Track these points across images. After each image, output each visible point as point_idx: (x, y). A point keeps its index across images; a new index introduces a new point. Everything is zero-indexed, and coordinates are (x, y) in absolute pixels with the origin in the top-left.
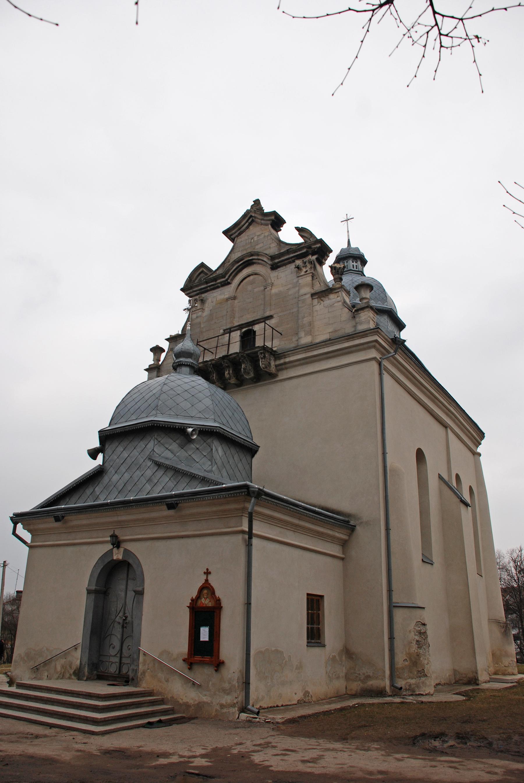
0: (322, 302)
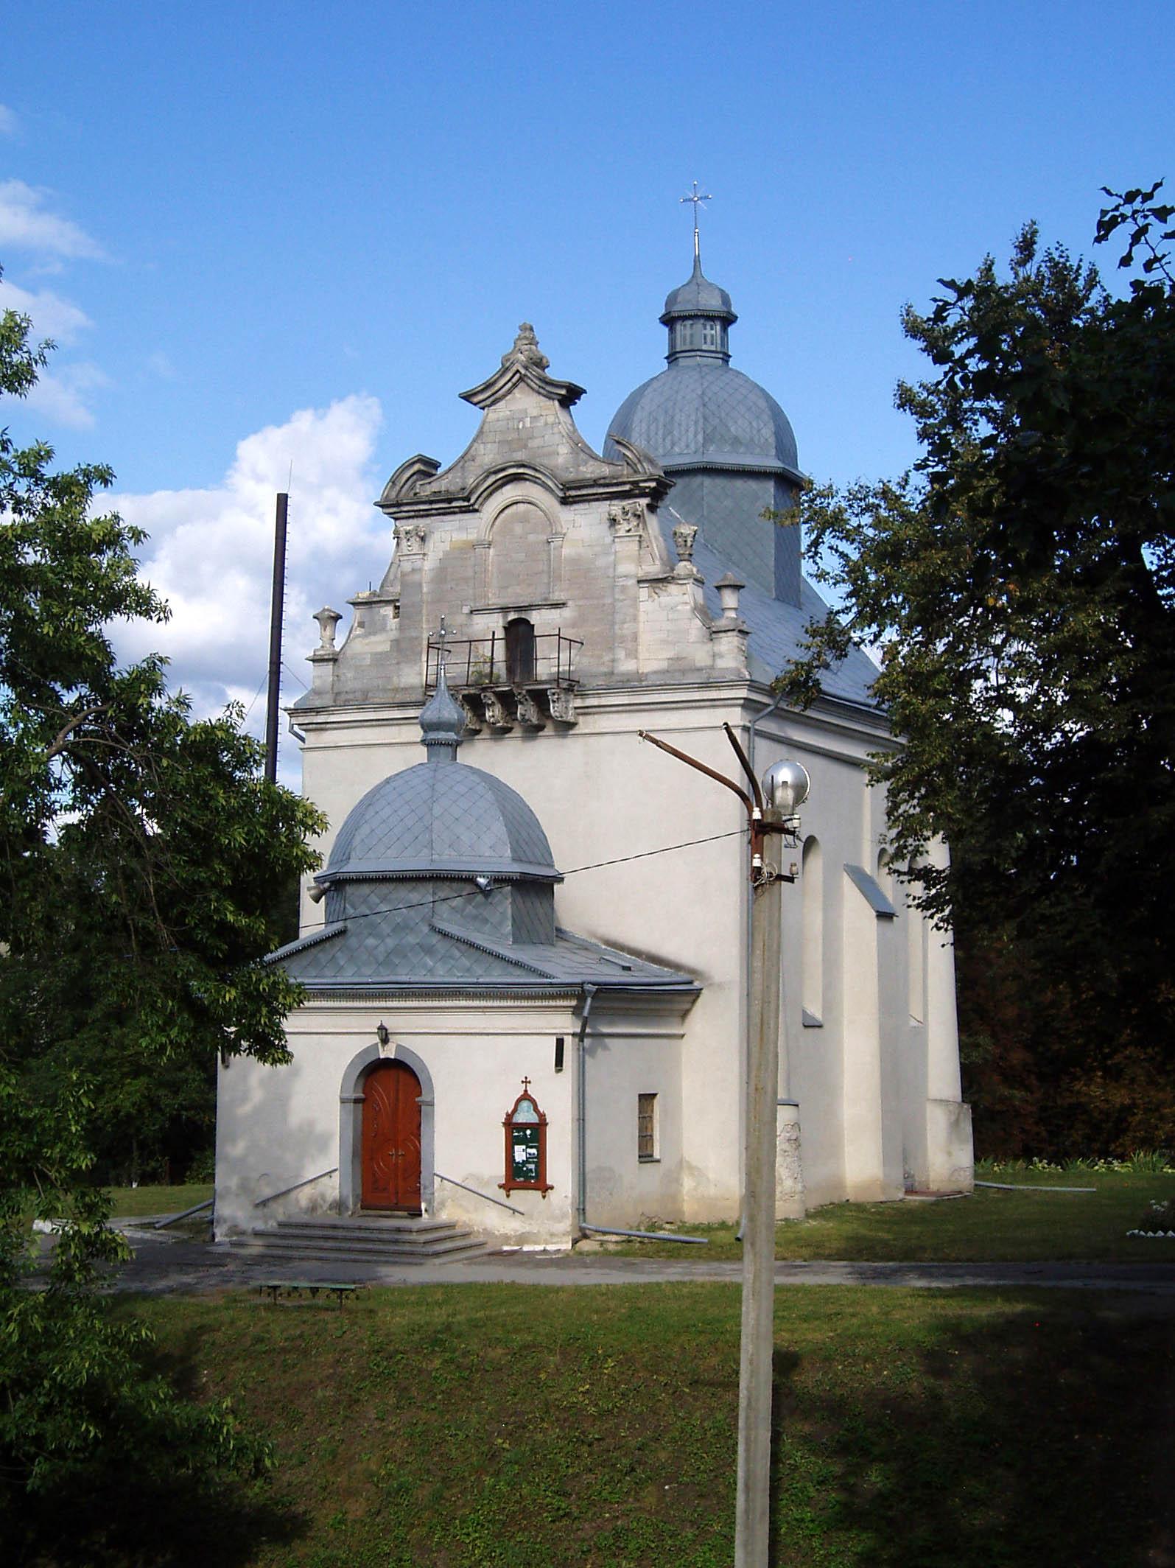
0: (656, 596)
